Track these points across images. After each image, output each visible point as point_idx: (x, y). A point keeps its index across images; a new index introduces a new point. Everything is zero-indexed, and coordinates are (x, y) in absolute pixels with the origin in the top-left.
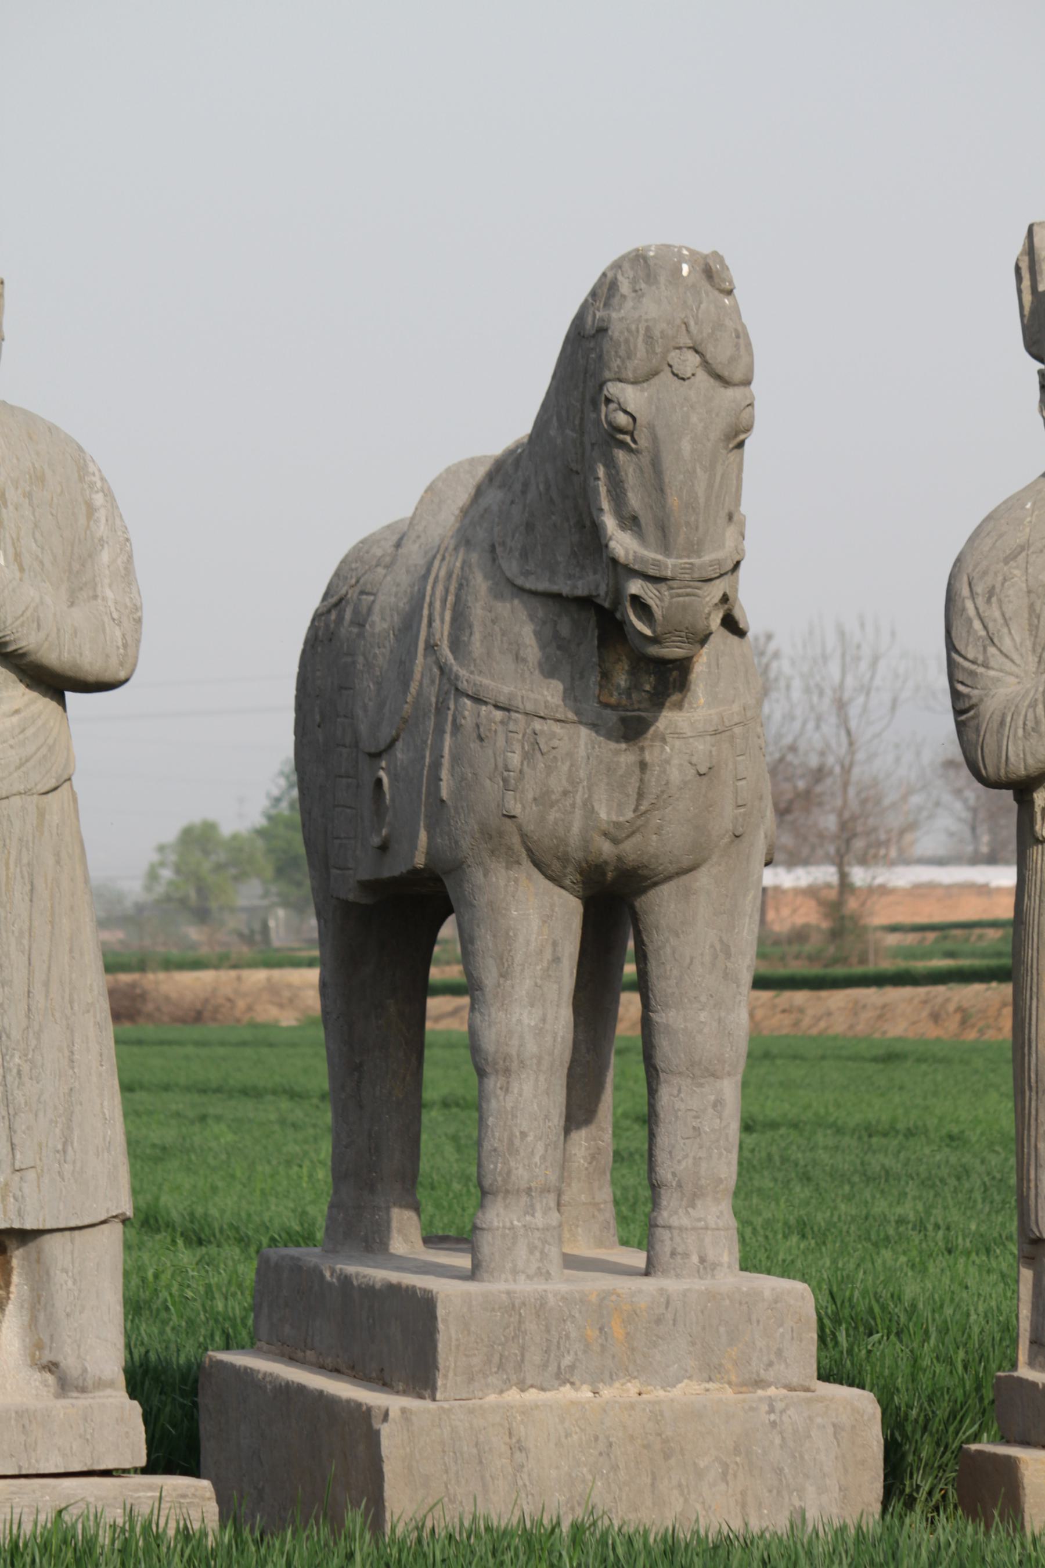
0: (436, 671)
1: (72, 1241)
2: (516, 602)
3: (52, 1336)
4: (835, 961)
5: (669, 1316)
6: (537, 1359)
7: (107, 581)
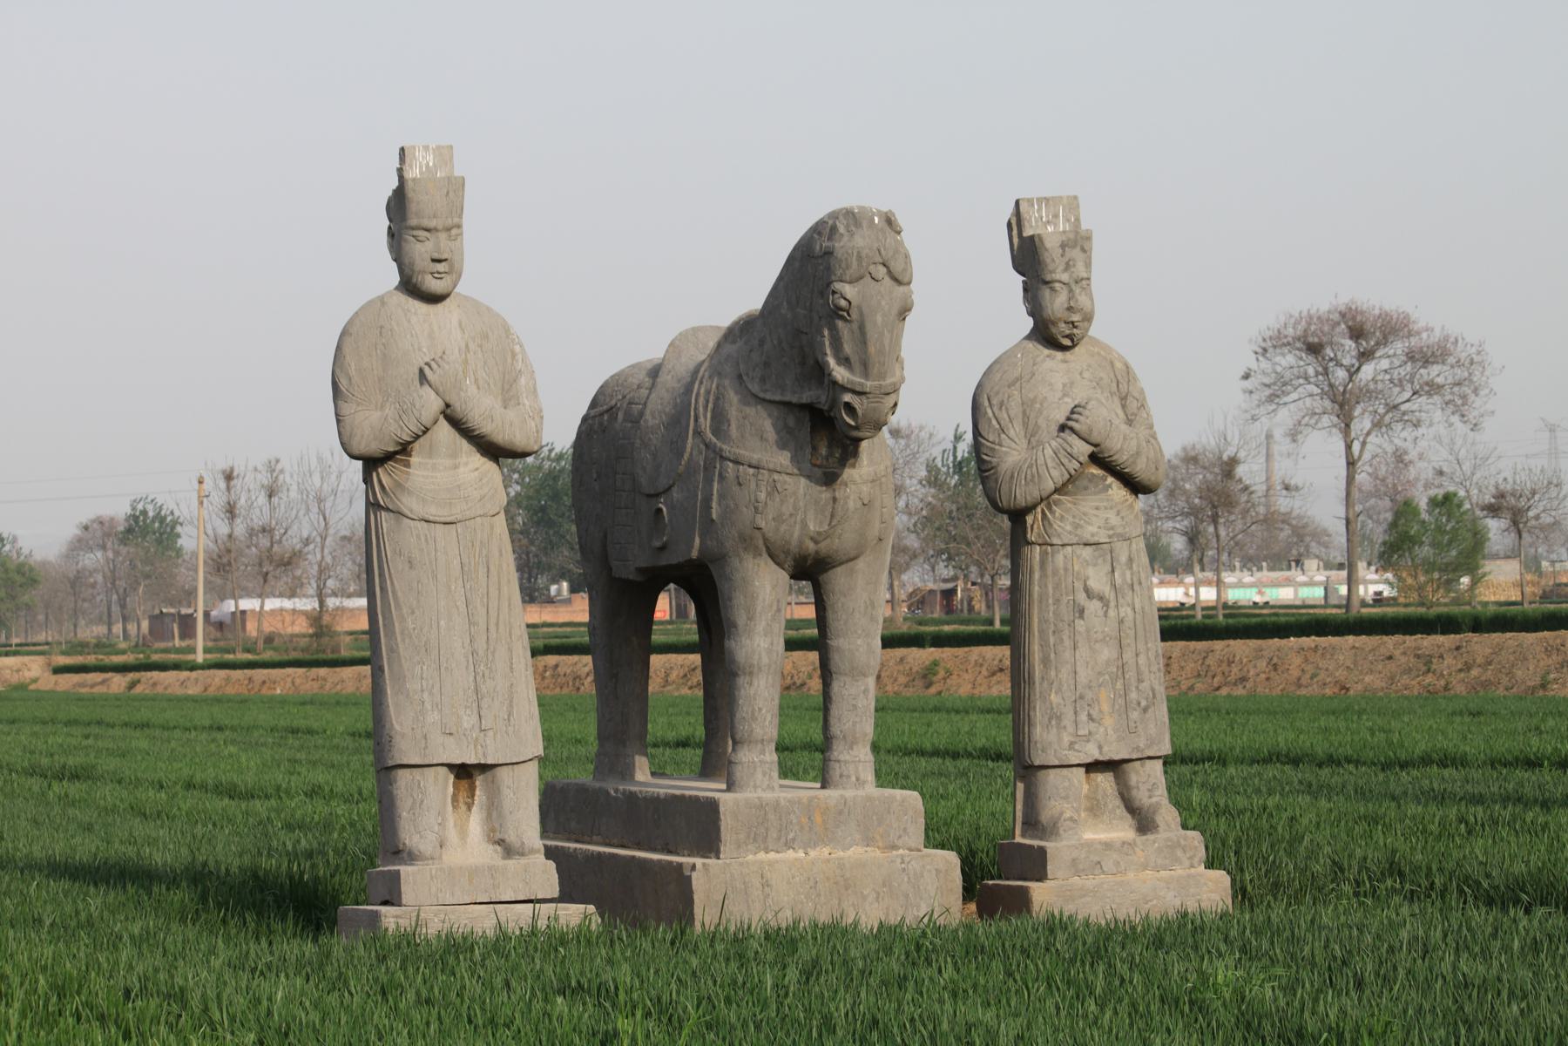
0: (702, 447)
1: (513, 770)
2: (759, 407)
3: (501, 825)
4: (318, 652)
5: (846, 811)
6: (775, 835)
7: (524, 395)
